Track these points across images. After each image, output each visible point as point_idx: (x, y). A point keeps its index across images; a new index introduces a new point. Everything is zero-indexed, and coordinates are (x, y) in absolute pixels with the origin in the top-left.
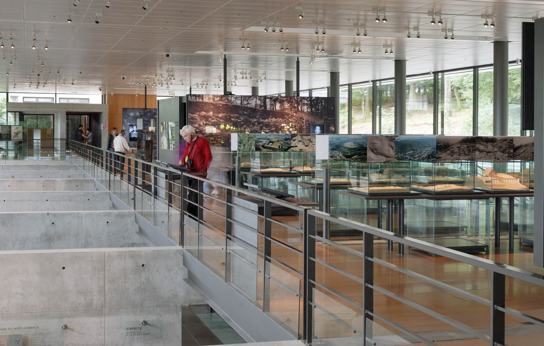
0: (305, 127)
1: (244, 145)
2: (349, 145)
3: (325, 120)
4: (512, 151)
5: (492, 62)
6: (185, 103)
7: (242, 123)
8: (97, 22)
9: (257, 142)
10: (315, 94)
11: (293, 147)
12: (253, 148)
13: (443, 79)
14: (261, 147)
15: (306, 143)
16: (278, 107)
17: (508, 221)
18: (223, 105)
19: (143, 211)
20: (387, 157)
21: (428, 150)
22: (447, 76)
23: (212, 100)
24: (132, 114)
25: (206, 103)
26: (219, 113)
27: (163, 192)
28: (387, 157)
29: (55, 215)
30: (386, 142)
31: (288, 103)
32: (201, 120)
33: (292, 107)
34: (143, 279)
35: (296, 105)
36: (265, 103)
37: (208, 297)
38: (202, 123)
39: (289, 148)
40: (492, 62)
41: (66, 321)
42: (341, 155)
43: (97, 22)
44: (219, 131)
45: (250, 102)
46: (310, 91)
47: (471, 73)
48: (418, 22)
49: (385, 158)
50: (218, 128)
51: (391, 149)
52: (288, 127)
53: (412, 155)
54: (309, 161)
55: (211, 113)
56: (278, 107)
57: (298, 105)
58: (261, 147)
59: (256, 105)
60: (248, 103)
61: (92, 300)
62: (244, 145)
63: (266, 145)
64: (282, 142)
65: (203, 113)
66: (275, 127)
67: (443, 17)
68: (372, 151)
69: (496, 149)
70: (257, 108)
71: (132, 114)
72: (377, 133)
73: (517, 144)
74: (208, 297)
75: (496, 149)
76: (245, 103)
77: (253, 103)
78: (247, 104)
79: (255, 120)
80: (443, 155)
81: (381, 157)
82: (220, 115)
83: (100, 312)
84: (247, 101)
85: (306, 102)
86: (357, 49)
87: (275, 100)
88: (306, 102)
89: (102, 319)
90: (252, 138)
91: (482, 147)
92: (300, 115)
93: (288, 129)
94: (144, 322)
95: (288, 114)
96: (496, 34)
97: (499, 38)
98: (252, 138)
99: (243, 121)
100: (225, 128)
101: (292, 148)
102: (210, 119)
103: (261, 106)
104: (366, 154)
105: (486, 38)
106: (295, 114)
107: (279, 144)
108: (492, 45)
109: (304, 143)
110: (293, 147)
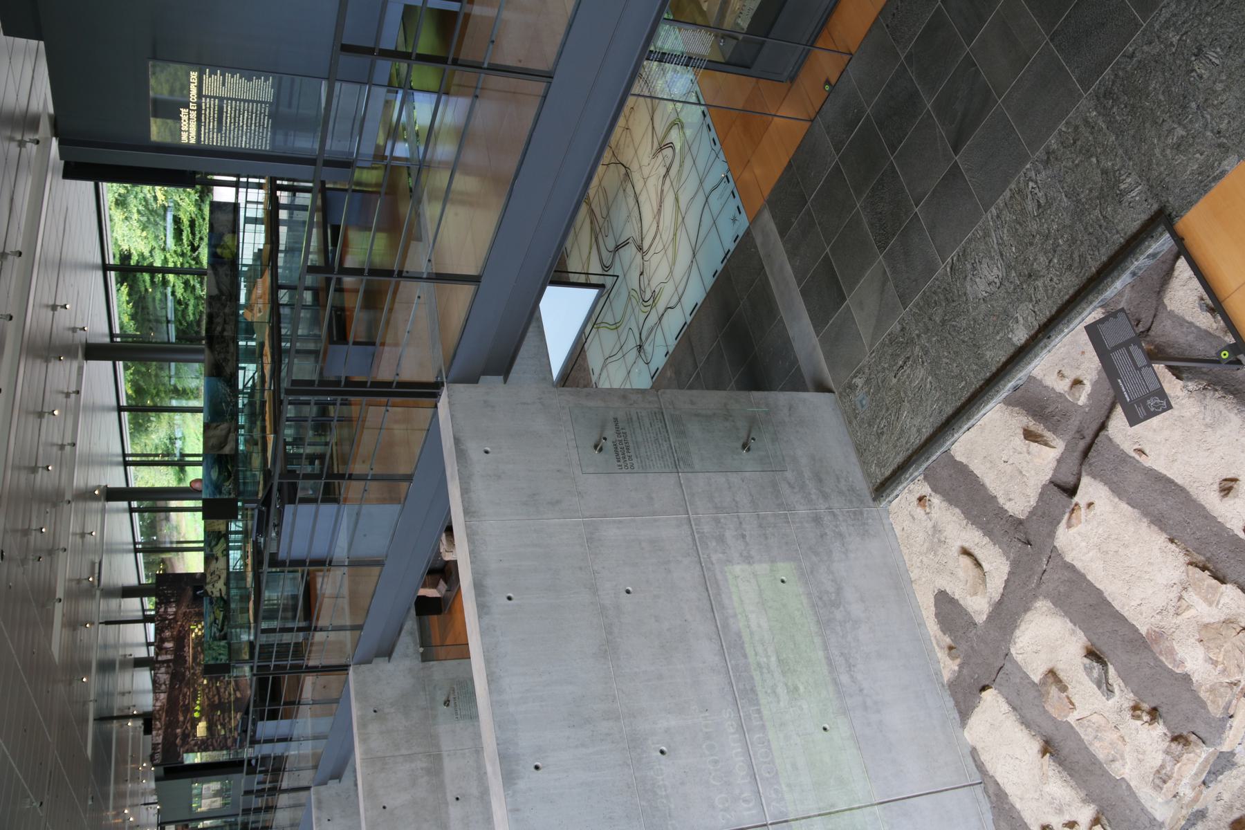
0: (197, 609)
1: (220, 654)
4: (224, 297)
5: (110, 363)
6: (165, 769)
7: (192, 690)
9: (215, 639)
11: (221, 594)
12: (223, 643)
14: (222, 633)
15: (216, 579)
17: (311, 663)
18: (166, 716)
19: (301, 752)
20: (229, 432)
21: (222, 388)
23: (160, 732)
26: (178, 721)
27: (278, 749)
28: (229, 432)
30: (211, 433)
31: (164, 632)
32: (188, 743)
34: (392, 710)
35: (167, 622)
38: (193, 742)
40: (110, 363)
42: (227, 484)
44: (203, 718)
45: (162, 681)
47: (131, 469)
48: (53, 445)
49: (231, 434)
50: (199, 720)
51: (219, 428)
52: (196, 630)
53: (228, 404)
55: (179, 731)
57: (167, 619)
58: (222, 633)
59: (167, 673)
60: (165, 683)
61: (422, 769)
62: (220, 654)
63: (219, 627)
64: (215, 607)
66: (197, 647)
68: (223, 448)
69: (221, 314)
70: (170, 671)
72: (201, 459)
73: (215, 292)
75: (221, 314)
76: (163, 687)
77: (164, 677)
78: (166, 685)
79: (187, 673)
80: (228, 370)
81: (230, 438)
82: (181, 718)
84: (161, 685)
85: (162, 610)
88: (162, 610)
89: (445, 754)
90: (210, 645)
91: (219, 329)
93: (199, 630)
94: (445, 704)
95: (180, 632)
96: (75, 357)
98: (210, 645)
99: (189, 689)
100: (199, 711)
101: (223, 595)
102: (187, 732)
103: (168, 667)
104: (226, 455)
105: (80, 369)
106: (179, 623)
107: (218, 612)
108: (90, 362)
109: (217, 581)
110: (221, 594)
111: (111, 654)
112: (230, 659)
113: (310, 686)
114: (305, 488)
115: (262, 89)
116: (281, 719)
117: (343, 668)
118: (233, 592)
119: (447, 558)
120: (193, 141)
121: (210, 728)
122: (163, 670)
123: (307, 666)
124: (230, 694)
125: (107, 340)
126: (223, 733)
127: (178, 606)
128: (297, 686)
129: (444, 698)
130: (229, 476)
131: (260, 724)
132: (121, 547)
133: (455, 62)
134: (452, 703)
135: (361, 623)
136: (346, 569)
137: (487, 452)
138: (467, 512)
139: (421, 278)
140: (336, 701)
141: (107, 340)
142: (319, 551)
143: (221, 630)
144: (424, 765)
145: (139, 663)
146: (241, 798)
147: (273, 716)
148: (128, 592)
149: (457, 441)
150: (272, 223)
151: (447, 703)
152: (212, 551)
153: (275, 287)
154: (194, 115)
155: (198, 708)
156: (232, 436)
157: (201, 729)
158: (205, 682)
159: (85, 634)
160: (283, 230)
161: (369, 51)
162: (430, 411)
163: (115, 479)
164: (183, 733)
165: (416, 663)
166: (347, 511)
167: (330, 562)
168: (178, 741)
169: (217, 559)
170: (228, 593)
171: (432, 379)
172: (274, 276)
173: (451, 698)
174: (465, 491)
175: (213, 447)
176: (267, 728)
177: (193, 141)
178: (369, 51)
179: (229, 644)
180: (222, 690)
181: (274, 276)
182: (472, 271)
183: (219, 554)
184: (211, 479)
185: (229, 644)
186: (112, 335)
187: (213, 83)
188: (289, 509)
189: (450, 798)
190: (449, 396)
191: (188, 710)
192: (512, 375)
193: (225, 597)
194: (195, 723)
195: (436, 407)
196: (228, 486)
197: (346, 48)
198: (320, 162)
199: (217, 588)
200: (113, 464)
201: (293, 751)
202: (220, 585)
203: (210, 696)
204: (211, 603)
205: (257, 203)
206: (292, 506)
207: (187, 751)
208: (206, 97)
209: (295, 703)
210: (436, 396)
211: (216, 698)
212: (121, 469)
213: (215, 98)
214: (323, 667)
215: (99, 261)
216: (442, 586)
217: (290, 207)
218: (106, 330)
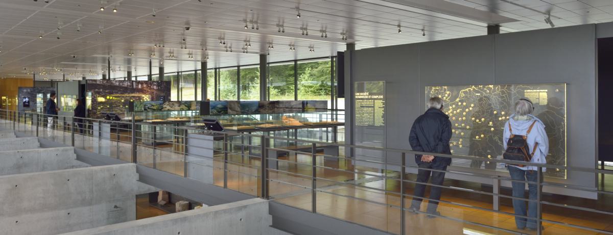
2: (219, 106)
3: (166, 93)
6: (84, 85)
8: (58, 38)
9: (145, 106)
10: (139, 79)
12: (143, 109)
13: (219, 71)
16: (140, 86)
20: (236, 111)
21: (254, 108)
22: (221, 70)
24: (25, 91)
25: (98, 84)
26: (106, 90)
27: (96, 133)
28: (236, 111)
29: (23, 153)
30: (236, 105)
33: (148, 86)
36: (132, 84)
37: (348, 171)
39: (162, 109)
40: (259, 62)
41: (69, 210)
43: (58, 38)
46: (136, 77)
47: (214, 71)
50: (106, 98)
53: (248, 111)
54: (146, 116)
56: (140, 86)
57: (151, 85)
59: (127, 86)
65: (97, 90)
67: (225, 40)
68: (230, 109)
70: (129, 86)
71: (25, 91)
74: (348, 171)
76: (121, 84)
77: (126, 84)
80: (261, 110)
81: (234, 112)
82: (107, 91)
83: (90, 203)
85: (155, 83)
86: (191, 56)
87: (142, 83)
88: (155, 83)
92: (153, 91)
96: (261, 51)
97: (262, 53)
103: (130, 86)
104: (227, 110)
105: (257, 53)
111: (133, 63)
112: (136, 112)
113: (127, 146)
114: (221, 144)
115: (379, 121)
116: (111, 134)
117: (135, 160)
118: (165, 113)
119: (177, 204)
120: (356, 97)
121: (101, 103)
122: (129, 84)
123: (136, 145)
124: (116, 111)
125: (267, 62)
126: (99, 108)
127: (157, 90)
128: (127, 139)
129: (118, 205)
130: (219, 112)
131: (109, 125)
132: (180, 66)
133: (315, 180)
134: (116, 209)
135: (157, 167)
136: (183, 160)
137: (241, 220)
138: (216, 212)
139: (403, 207)
140: (118, 158)
141: (267, 62)
142: (192, 150)
143: (148, 108)
144: (87, 198)
145: (129, 73)
146: (63, 116)
147: (112, 130)
148: (161, 69)
149: (245, 207)
150: (321, 125)
151: (116, 207)
152: (183, 104)
153: (296, 128)
154: (367, 97)
155: (111, 98)
156: (235, 112)
157: (101, 99)
158: (123, 101)
159: (144, 54)
160: (318, 129)
161: (404, 163)
162: (255, 193)
163: (210, 65)
164: (101, 92)
165: (136, 192)
166: (211, 162)
167: (187, 155)
168: (97, 90)
169: (179, 106)
170: (165, 111)
171: (271, 194)
172: (300, 127)
173: (118, 209)
174: (225, 211)
175: (230, 105)
176: (107, 128)
177: (356, 97)
178: (404, 163)
179: (143, 111)
180: (118, 108)
181: (300, 127)
182: (318, 209)
183: (181, 107)
184: (217, 105)
185: (143, 111)
186: (269, 63)
187: (379, 104)
188: (212, 138)
189: (69, 210)
190: (264, 202)
191: (110, 93)
192: (273, 229)
193: (163, 110)
194: (104, 96)
195: (258, 197)
196: (215, 111)
197: (404, 154)
198: (352, 146)
199: (167, 106)
200: (216, 63)
201: (96, 139)
202: (168, 107)
203: (116, 103)
204: (161, 104)
205: (327, 118)
206: (213, 139)
207: (92, 94)
208: (374, 101)
209: (119, 139)
210: (263, 196)
211: (115, 106)
212: (214, 67)
213: (374, 105)
214: (136, 152)
215: (298, 59)
216: (163, 203)
217: (327, 132)
218: (270, 62)
